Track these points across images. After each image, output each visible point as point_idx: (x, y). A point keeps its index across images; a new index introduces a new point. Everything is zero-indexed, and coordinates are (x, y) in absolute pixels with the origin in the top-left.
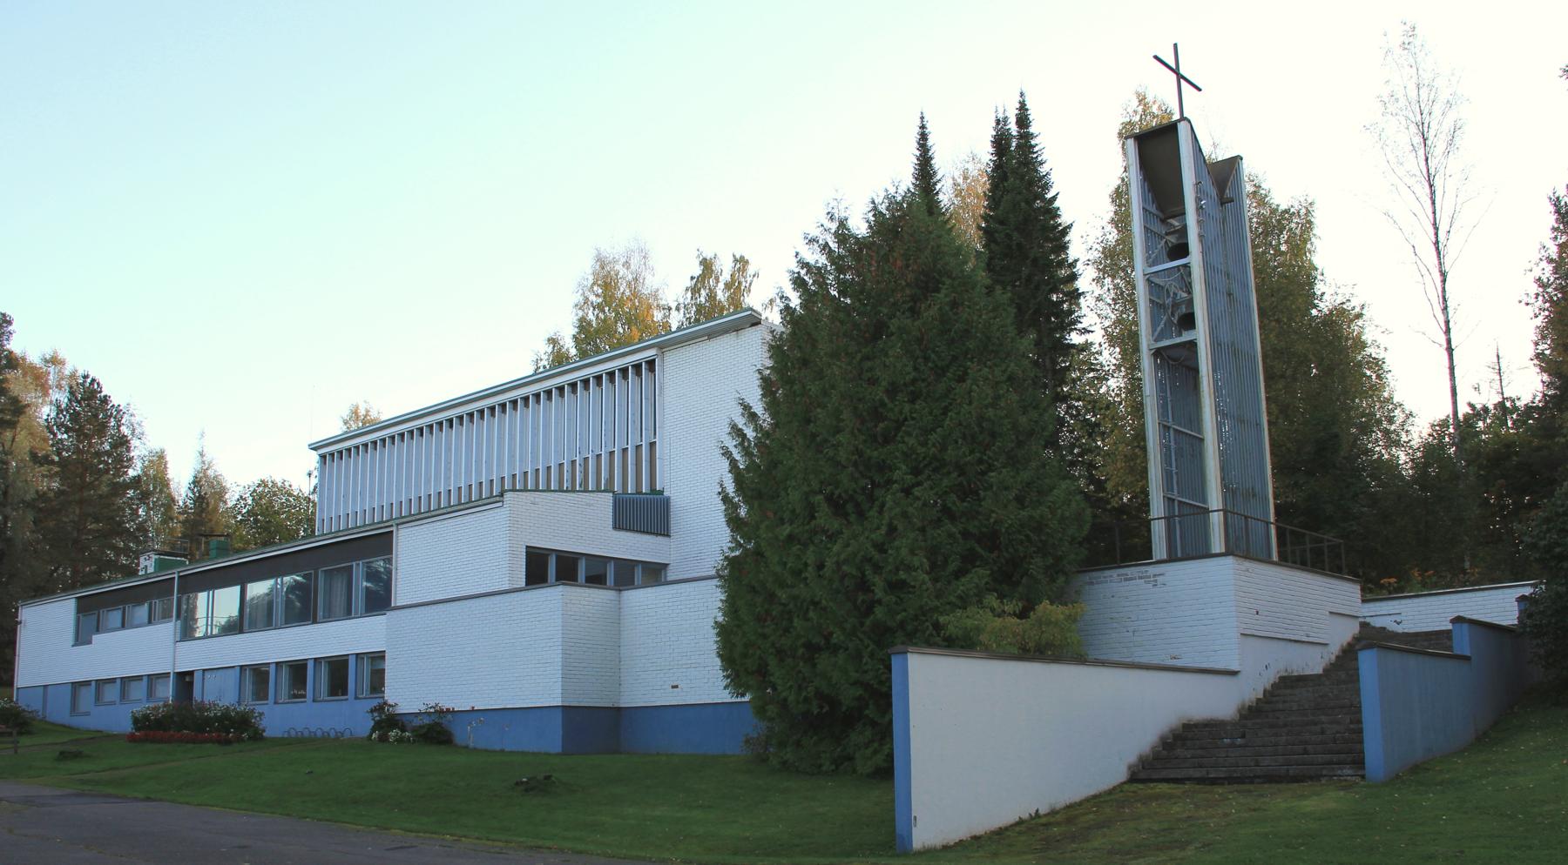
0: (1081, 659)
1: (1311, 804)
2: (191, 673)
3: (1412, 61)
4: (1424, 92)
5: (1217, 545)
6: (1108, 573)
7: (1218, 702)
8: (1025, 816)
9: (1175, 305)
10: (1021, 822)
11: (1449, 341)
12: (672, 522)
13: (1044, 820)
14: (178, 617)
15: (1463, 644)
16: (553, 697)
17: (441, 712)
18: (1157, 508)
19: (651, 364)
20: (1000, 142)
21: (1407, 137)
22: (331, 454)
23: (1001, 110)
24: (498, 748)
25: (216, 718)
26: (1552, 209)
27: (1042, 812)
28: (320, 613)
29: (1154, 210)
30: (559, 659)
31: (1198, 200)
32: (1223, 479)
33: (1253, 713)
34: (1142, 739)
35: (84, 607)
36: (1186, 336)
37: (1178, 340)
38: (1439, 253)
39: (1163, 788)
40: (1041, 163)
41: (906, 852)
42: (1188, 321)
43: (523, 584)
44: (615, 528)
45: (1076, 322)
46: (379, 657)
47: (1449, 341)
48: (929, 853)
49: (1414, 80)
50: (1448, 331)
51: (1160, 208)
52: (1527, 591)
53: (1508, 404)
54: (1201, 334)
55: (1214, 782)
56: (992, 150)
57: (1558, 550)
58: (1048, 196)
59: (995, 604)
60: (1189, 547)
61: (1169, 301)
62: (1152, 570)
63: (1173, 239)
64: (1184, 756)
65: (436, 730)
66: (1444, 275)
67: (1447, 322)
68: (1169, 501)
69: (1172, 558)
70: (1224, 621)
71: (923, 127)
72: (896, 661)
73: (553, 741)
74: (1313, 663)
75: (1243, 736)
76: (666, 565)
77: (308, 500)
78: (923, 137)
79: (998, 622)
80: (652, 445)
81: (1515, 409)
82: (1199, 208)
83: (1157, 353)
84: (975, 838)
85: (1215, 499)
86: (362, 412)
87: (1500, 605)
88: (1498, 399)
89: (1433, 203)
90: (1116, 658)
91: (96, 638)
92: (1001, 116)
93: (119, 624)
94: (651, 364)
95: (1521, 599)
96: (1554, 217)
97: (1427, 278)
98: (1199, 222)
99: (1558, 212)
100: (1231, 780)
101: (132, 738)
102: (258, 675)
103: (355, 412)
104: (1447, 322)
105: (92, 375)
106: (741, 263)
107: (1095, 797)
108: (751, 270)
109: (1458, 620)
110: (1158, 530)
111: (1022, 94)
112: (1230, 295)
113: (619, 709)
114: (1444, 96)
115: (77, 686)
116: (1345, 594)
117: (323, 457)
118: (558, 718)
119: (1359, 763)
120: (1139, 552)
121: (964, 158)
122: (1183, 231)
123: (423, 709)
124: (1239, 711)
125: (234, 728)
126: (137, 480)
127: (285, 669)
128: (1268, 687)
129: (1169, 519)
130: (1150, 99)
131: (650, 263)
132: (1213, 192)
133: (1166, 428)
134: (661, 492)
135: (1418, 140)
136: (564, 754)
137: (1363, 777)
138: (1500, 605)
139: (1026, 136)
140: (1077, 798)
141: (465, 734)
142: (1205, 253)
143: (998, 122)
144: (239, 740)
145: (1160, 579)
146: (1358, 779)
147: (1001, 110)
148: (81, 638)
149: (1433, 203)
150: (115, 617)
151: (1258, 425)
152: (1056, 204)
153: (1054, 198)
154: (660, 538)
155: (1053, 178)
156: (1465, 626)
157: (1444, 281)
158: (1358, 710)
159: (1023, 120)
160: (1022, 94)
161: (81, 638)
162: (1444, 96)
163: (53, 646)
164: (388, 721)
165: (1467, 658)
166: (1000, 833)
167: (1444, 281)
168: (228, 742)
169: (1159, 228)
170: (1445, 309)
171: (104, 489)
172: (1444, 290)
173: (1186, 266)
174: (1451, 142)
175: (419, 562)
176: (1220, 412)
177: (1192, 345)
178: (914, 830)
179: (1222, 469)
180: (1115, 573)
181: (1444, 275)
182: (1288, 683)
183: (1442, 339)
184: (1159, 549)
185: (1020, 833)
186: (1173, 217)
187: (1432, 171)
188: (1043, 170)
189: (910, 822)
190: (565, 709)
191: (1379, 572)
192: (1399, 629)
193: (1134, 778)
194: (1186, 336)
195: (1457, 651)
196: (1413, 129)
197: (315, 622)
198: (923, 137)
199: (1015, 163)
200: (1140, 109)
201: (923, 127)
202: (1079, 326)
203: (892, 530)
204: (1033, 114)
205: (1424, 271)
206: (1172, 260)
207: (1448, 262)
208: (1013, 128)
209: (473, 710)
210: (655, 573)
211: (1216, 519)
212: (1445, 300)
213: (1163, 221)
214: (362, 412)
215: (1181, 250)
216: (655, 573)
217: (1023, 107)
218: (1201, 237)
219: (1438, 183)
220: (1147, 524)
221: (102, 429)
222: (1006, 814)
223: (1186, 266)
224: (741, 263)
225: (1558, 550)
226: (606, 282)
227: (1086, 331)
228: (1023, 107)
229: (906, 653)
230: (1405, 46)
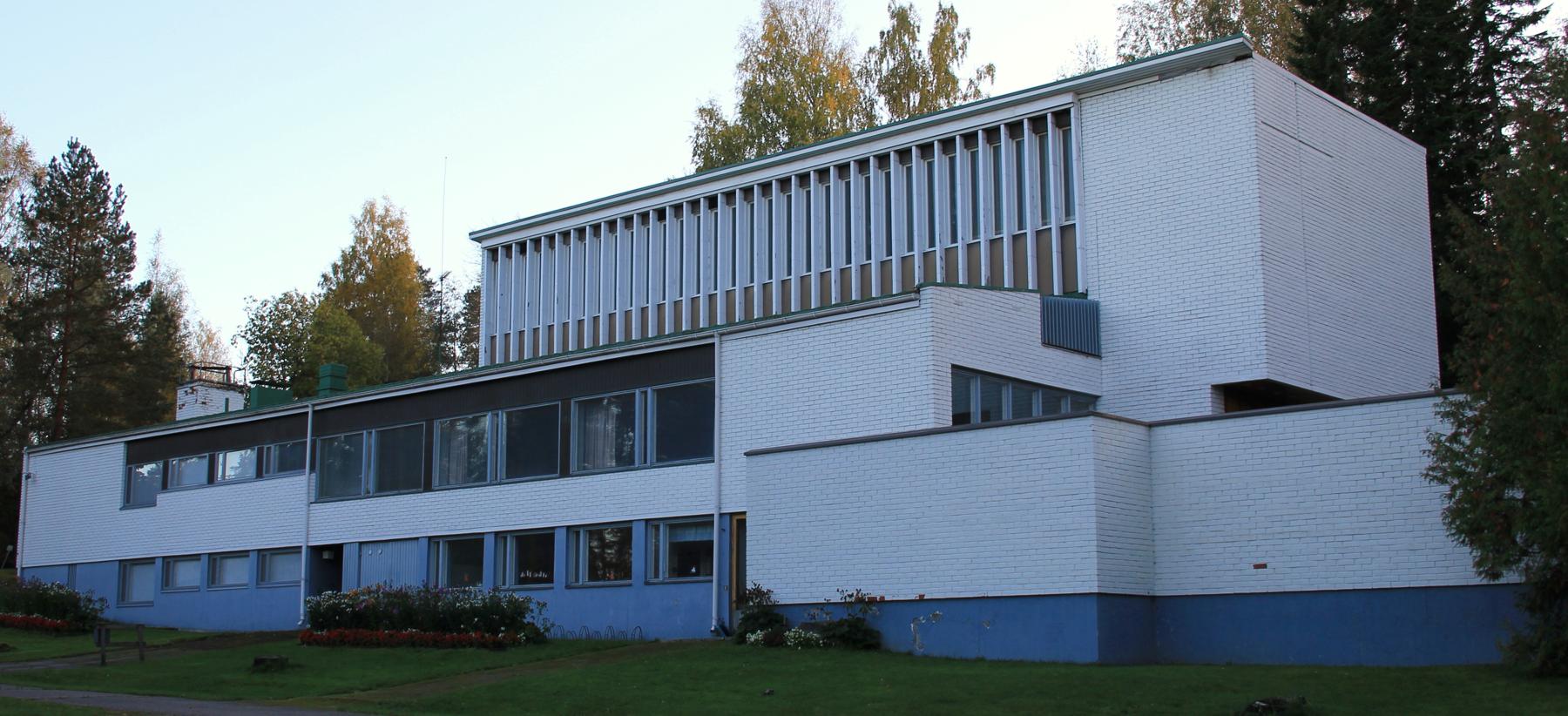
2: (337, 550)
12: (1103, 336)
14: (312, 469)
16: (1087, 581)
17: (865, 603)
19: (1062, 117)
22: (504, 247)
24: (972, 654)
25: (474, 611)
28: (573, 466)
30: (1091, 525)
35: (137, 454)
43: (948, 422)
44: (1048, 342)
46: (738, 523)
65: (855, 628)
73: (1083, 644)
76: (1097, 398)
80: (1067, 231)
86: (380, 211)
91: (163, 498)
93: (204, 479)
94: (1062, 117)
101: (307, 638)
102: (534, 549)
103: (370, 213)
105: (83, 143)
106: (948, 16)
108: (960, 28)
113: (1153, 598)
115: (126, 566)
117: (493, 252)
118: (1093, 609)
123: (837, 598)
125: (501, 627)
126: (145, 289)
127: (443, 548)
131: (836, 11)
134: (1085, 295)
136: (1101, 664)
141: (893, 636)
144: (516, 643)
148: (135, 496)
150: (194, 466)
154: (1090, 360)
161: (135, 496)
163: (76, 508)
164: (762, 617)
168: (499, 646)
171: (97, 300)
175: (756, 384)
190: (1103, 598)
197: (565, 473)
209: (921, 599)
210: (1084, 405)
214: (380, 211)
216: (1084, 405)
221: (96, 223)
224: (948, 16)
226: (776, 34)
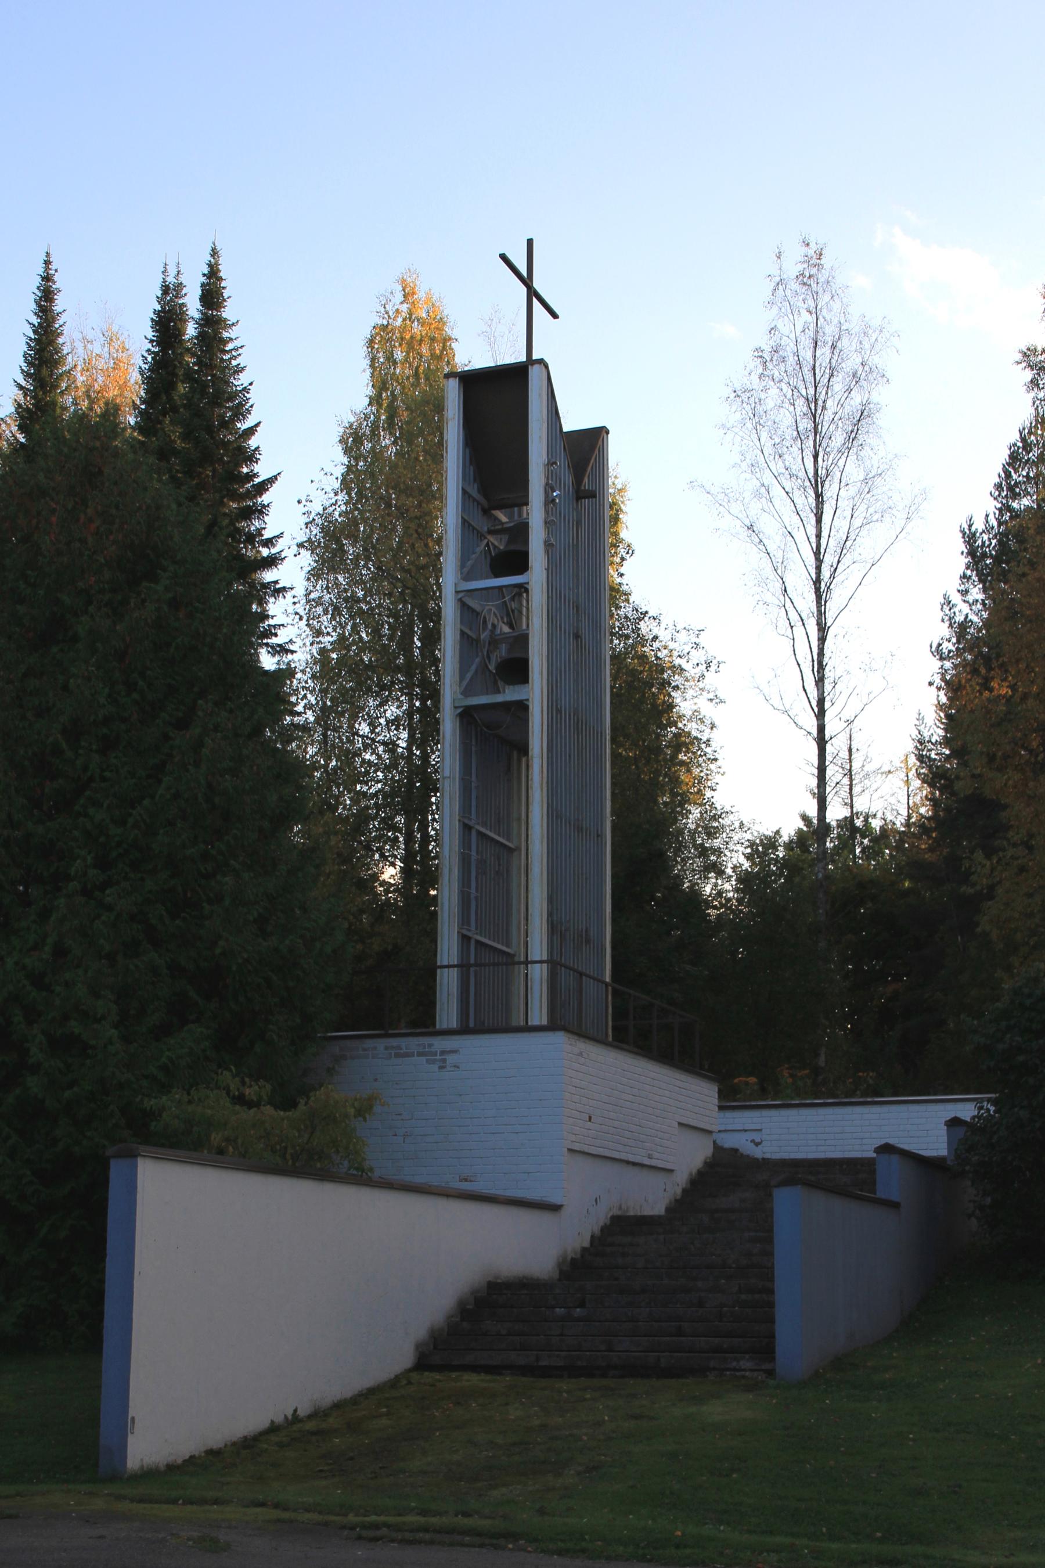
0: (361, 1176)
1: (715, 1411)
3: (811, 303)
4: (824, 353)
5: (539, 1015)
6: (369, 1043)
7: (530, 1248)
8: (279, 1419)
9: (494, 642)
10: (273, 1429)
11: (821, 729)
13: (310, 1426)
15: (892, 1183)
18: (448, 948)
20: (167, 322)
21: (787, 418)
23: (172, 271)
26: (963, 548)
27: (301, 1413)
29: (475, 493)
31: (549, 488)
32: (550, 914)
33: (577, 1268)
34: (433, 1304)
36: (511, 694)
37: (499, 698)
38: (819, 597)
39: (471, 1380)
40: (239, 370)
41: (117, 1476)
42: (516, 670)
45: (269, 633)
47: (821, 729)
48: (148, 1474)
49: (811, 333)
50: (821, 714)
51: (484, 490)
52: (967, 1111)
53: (859, 823)
54: (536, 692)
55: (546, 1372)
56: (151, 334)
57: (1021, 1058)
58: (243, 426)
59: (234, 1085)
60: (489, 1017)
61: (484, 636)
62: (440, 1043)
63: (499, 543)
64: (490, 1330)
66: (823, 630)
67: (821, 702)
68: (465, 939)
69: (464, 1030)
70: (562, 1129)
71: (47, 278)
72: (116, 1169)
74: (653, 1198)
75: (582, 1305)
77: (979, 1117)
78: (46, 296)
79: (248, 1115)
81: (867, 830)
82: (549, 501)
83: (467, 716)
84: (210, 1452)
85: (538, 947)
87: (925, 1126)
88: (846, 812)
89: (819, 520)
90: (419, 1179)
92: (171, 279)
95: (954, 1123)
96: (964, 560)
97: (799, 630)
98: (547, 523)
99: (972, 553)
100: (572, 1371)
104: (821, 702)
107: (371, 1391)
109: (886, 1149)
110: (448, 982)
111: (214, 253)
112: (577, 636)
114: (852, 363)
116: (694, 1096)
119: (765, 1350)
120: (423, 1021)
121: (111, 345)
122: (522, 530)
124: (560, 1265)
128: (597, 1230)
129: (463, 966)
130: (421, 294)
132: (569, 479)
133: (466, 828)
135: (806, 424)
137: (771, 1373)
138: (925, 1126)
139: (213, 325)
140: (348, 1393)
142: (551, 569)
143: (166, 289)
145: (451, 1059)
146: (761, 1376)
147: (172, 271)
149: (819, 520)
151: (600, 836)
152: (253, 442)
153: (251, 431)
155: (253, 396)
156: (895, 1158)
157: (822, 640)
158: (768, 1274)
159: (212, 296)
160: (214, 253)
162: (852, 363)
165: (895, 1205)
166: (249, 1444)
167: (822, 640)
169: (481, 524)
170: (820, 681)
172: (821, 653)
173: (467, 577)
174: (852, 437)
176: (554, 815)
177: (522, 707)
178: (131, 1439)
179: (550, 900)
180: (381, 1044)
181: (823, 630)
182: (622, 1227)
183: (812, 725)
184: (447, 1014)
185: (281, 1445)
186: (499, 508)
187: (822, 472)
188: (242, 380)
189: (124, 1426)
191: (745, 1071)
192: (758, 1153)
193: (423, 1363)
194: (511, 694)
195: (881, 1194)
196: (801, 405)
198: (46, 296)
199: (193, 364)
200: (404, 308)
201: (47, 278)
202: (274, 640)
203: (60, 952)
204: (230, 287)
205: (794, 616)
206: (497, 575)
207: (832, 608)
208: (193, 305)
211: (538, 974)
212: (821, 667)
213: (486, 512)
215: (515, 561)
217: (213, 273)
218: (548, 545)
219: (830, 491)
220: (430, 972)
222: (251, 1420)
223: (467, 577)
225: (1021, 1058)
227: (282, 650)
228: (213, 273)
229: (133, 1155)
230: (805, 280)
